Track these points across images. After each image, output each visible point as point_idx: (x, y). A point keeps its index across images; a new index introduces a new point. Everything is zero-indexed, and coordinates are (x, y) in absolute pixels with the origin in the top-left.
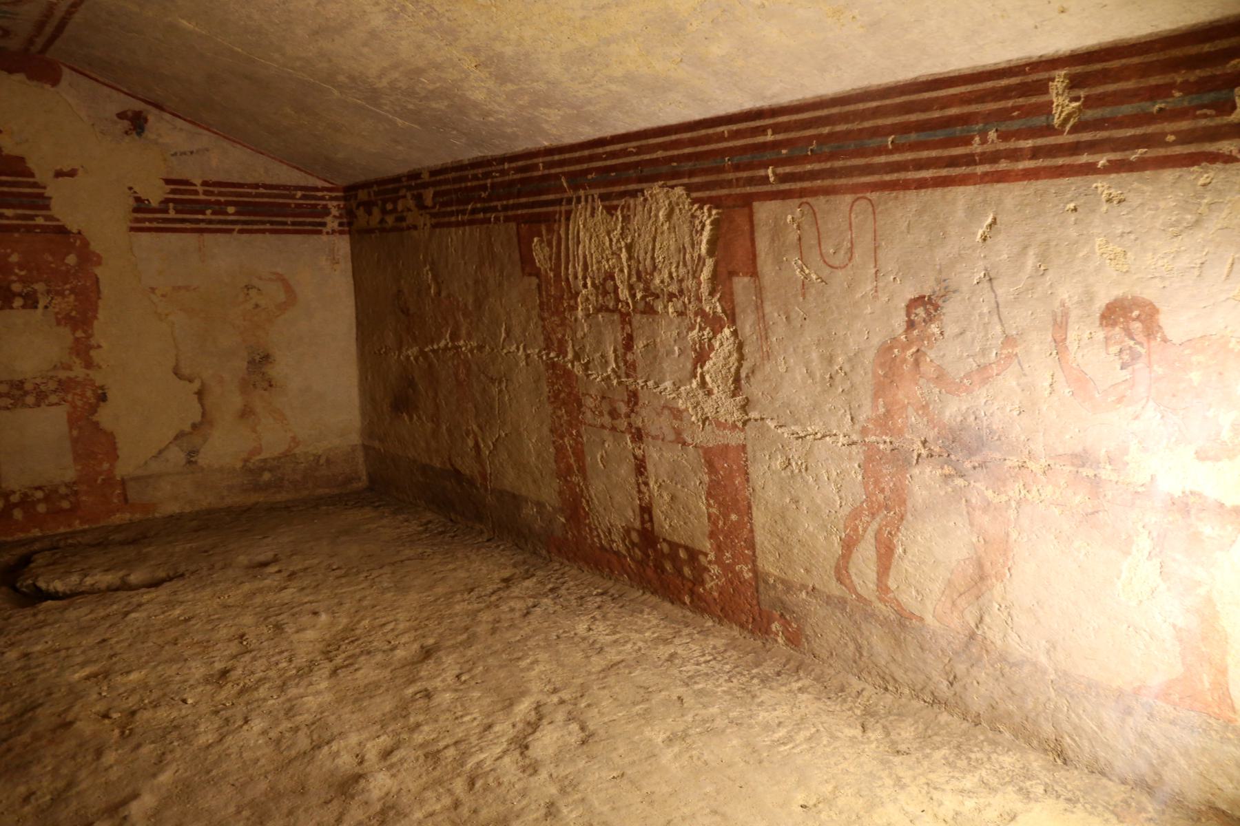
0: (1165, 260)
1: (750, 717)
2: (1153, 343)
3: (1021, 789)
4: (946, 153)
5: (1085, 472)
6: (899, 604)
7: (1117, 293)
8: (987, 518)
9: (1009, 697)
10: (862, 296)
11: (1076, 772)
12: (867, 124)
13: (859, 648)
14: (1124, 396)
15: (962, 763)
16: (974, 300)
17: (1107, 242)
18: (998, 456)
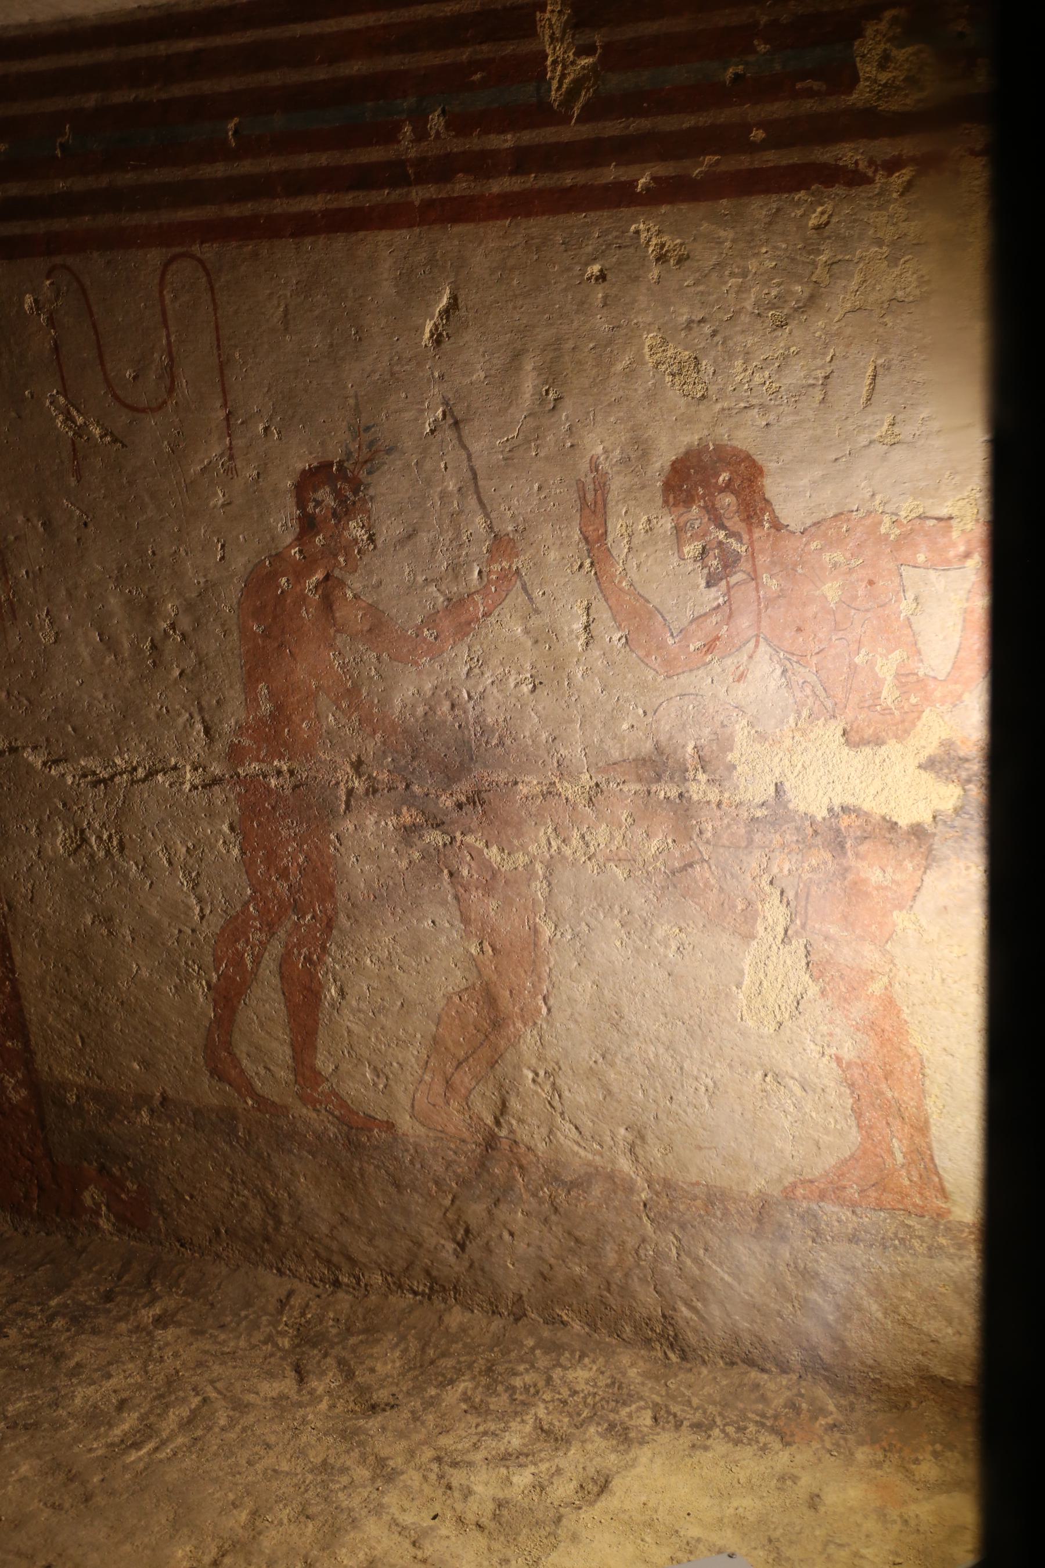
1: (55, 1404)
2: (757, 533)
3: (612, 1426)
4: (349, 158)
5: (667, 790)
6: (343, 1104)
7: (689, 439)
8: (493, 904)
9: (571, 1250)
10: (204, 470)
11: (705, 1371)
12: (180, 91)
13: (272, 1208)
14: (718, 638)
15: (499, 1402)
16: (428, 465)
17: (664, 341)
18: (503, 777)
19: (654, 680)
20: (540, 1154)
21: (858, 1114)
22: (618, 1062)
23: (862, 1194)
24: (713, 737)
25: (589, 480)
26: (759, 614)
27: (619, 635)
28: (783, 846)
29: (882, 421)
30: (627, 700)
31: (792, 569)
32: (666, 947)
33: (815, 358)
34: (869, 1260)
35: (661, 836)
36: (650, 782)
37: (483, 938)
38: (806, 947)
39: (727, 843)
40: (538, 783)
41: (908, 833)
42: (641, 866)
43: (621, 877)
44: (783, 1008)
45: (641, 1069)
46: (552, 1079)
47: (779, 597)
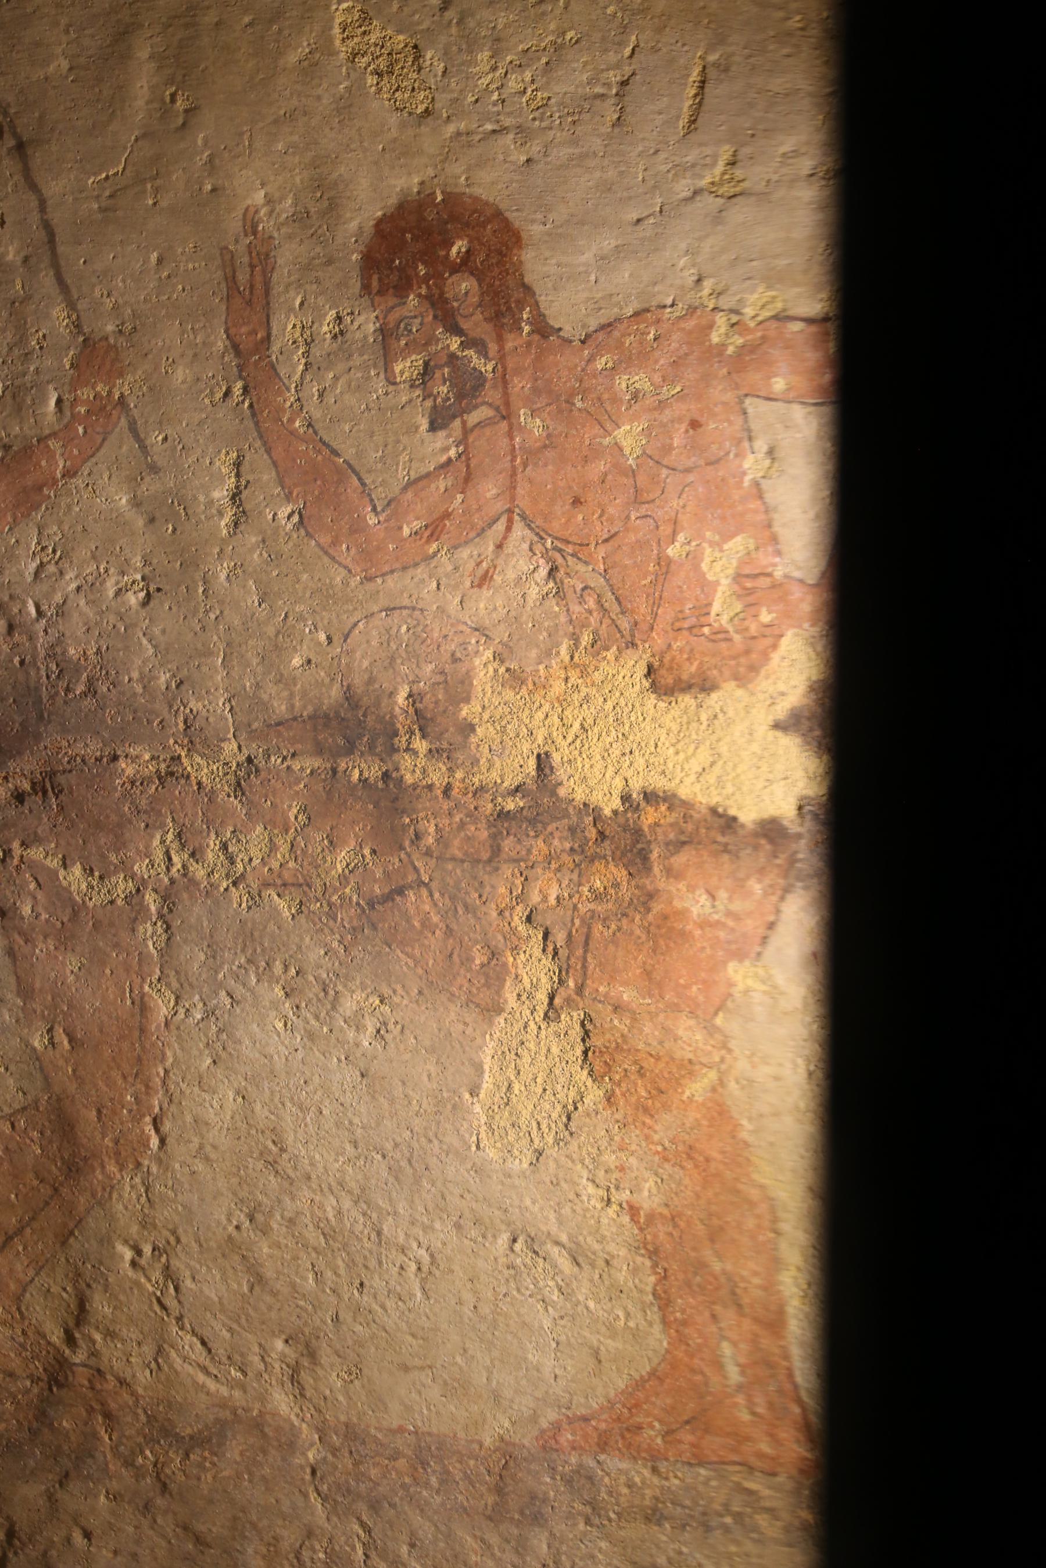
0: (528, 75)
8: (72, 963)
14: (447, 515)
17: (366, 18)
19: (345, 583)
20: (140, 1391)
21: (663, 1301)
22: (275, 1226)
23: (669, 1438)
24: (440, 678)
25: (241, 248)
26: (514, 474)
27: (289, 510)
28: (549, 858)
29: (715, 157)
30: (301, 618)
31: (567, 402)
32: (358, 1029)
33: (606, 50)
34: (680, 1553)
35: (352, 843)
36: (336, 754)
37: (54, 1022)
38: (583, 1025)
39: (459, 854)
40: (153, 758)
41: (756, 834)
42: (319, 894)
43: (286, 914)
44: (544, 1126)
45: (313, 1236)
46: (164, 1259)
47: (545, 447)
